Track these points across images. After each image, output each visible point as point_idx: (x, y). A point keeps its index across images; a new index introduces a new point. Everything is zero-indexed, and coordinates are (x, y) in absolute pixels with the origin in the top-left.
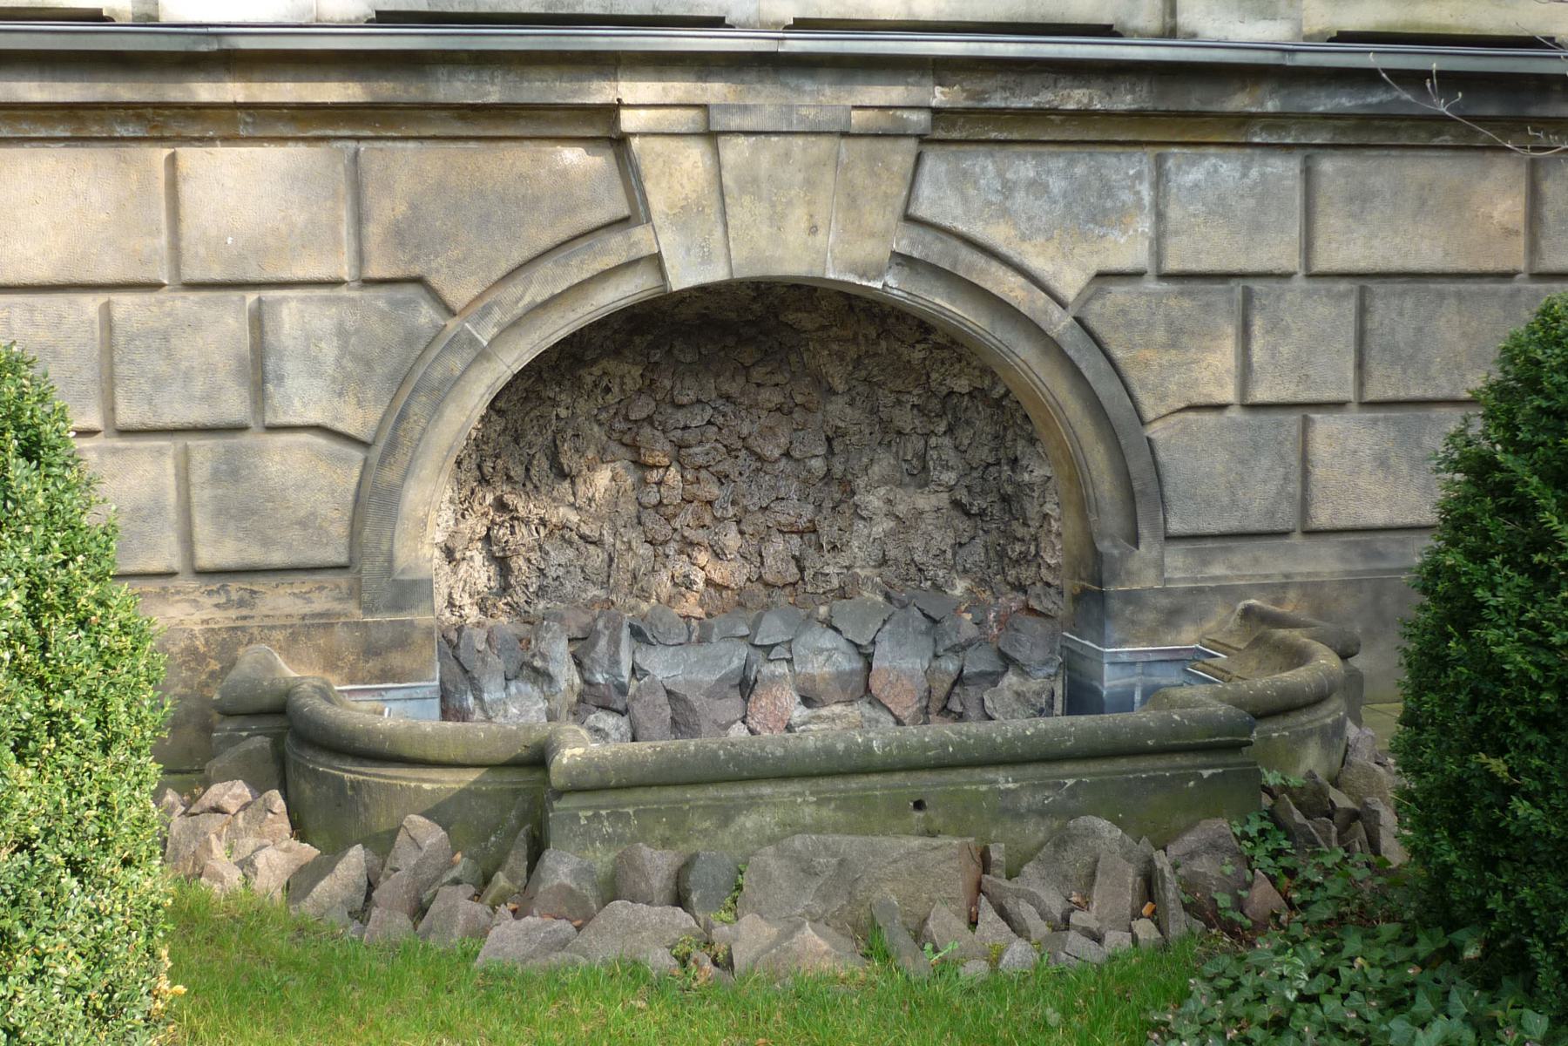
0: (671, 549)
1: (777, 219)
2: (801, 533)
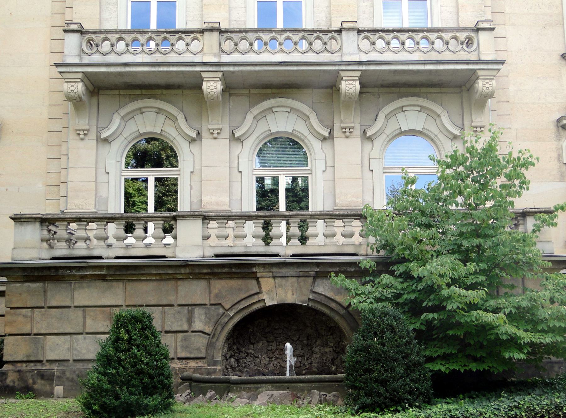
0: (273, 359)
1: (286, 293)
2: (301, 356)
